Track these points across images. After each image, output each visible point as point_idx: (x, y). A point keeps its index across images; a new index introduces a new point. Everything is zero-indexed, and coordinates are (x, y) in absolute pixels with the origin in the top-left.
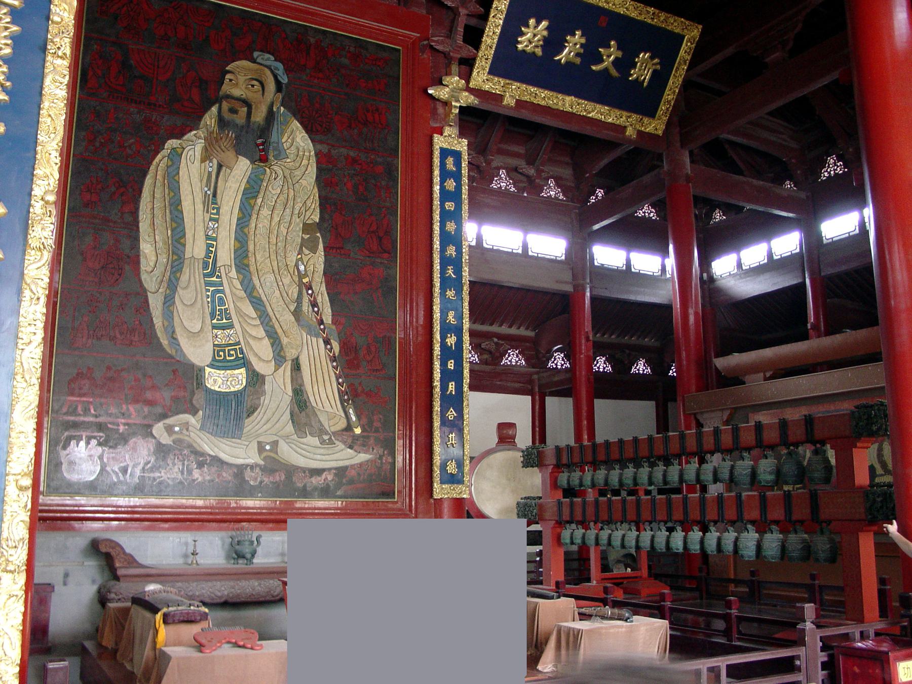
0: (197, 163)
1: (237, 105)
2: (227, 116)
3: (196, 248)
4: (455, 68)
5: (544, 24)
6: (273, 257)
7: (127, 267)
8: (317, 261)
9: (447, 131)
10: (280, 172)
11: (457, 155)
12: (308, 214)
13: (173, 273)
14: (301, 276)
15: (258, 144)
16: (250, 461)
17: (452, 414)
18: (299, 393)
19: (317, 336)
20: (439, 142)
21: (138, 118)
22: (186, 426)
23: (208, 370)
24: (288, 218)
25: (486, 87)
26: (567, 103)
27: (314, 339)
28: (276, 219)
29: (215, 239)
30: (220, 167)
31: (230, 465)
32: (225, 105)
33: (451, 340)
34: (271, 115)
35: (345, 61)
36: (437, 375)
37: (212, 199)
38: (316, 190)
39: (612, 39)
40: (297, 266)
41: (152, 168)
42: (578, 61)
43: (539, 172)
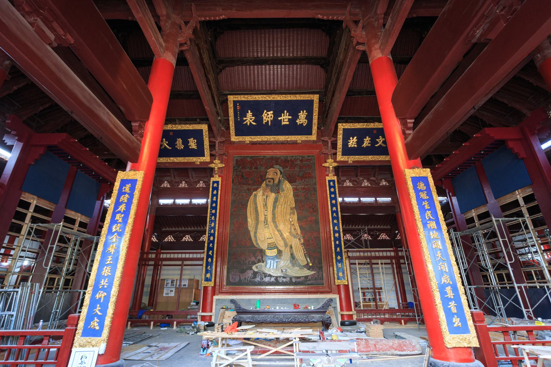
2: (268, 183)
3: (262, 218)
4: (330, 157)
5: (355, 138)
8: (295, 217)
9: (330, 175)
11: (334, 181)
15: (276, 188)
16: (279, 275)
17: (339, 258)
18: (292, 255)
20: (328, 178)
21: (246, 188)
25: (342, 160)
26: (370, 158)
33: (337, 235)
35: (299, 162)
36: (333, 246)
37: (265, 205)
42: (370, 145)
43: (377, 178)
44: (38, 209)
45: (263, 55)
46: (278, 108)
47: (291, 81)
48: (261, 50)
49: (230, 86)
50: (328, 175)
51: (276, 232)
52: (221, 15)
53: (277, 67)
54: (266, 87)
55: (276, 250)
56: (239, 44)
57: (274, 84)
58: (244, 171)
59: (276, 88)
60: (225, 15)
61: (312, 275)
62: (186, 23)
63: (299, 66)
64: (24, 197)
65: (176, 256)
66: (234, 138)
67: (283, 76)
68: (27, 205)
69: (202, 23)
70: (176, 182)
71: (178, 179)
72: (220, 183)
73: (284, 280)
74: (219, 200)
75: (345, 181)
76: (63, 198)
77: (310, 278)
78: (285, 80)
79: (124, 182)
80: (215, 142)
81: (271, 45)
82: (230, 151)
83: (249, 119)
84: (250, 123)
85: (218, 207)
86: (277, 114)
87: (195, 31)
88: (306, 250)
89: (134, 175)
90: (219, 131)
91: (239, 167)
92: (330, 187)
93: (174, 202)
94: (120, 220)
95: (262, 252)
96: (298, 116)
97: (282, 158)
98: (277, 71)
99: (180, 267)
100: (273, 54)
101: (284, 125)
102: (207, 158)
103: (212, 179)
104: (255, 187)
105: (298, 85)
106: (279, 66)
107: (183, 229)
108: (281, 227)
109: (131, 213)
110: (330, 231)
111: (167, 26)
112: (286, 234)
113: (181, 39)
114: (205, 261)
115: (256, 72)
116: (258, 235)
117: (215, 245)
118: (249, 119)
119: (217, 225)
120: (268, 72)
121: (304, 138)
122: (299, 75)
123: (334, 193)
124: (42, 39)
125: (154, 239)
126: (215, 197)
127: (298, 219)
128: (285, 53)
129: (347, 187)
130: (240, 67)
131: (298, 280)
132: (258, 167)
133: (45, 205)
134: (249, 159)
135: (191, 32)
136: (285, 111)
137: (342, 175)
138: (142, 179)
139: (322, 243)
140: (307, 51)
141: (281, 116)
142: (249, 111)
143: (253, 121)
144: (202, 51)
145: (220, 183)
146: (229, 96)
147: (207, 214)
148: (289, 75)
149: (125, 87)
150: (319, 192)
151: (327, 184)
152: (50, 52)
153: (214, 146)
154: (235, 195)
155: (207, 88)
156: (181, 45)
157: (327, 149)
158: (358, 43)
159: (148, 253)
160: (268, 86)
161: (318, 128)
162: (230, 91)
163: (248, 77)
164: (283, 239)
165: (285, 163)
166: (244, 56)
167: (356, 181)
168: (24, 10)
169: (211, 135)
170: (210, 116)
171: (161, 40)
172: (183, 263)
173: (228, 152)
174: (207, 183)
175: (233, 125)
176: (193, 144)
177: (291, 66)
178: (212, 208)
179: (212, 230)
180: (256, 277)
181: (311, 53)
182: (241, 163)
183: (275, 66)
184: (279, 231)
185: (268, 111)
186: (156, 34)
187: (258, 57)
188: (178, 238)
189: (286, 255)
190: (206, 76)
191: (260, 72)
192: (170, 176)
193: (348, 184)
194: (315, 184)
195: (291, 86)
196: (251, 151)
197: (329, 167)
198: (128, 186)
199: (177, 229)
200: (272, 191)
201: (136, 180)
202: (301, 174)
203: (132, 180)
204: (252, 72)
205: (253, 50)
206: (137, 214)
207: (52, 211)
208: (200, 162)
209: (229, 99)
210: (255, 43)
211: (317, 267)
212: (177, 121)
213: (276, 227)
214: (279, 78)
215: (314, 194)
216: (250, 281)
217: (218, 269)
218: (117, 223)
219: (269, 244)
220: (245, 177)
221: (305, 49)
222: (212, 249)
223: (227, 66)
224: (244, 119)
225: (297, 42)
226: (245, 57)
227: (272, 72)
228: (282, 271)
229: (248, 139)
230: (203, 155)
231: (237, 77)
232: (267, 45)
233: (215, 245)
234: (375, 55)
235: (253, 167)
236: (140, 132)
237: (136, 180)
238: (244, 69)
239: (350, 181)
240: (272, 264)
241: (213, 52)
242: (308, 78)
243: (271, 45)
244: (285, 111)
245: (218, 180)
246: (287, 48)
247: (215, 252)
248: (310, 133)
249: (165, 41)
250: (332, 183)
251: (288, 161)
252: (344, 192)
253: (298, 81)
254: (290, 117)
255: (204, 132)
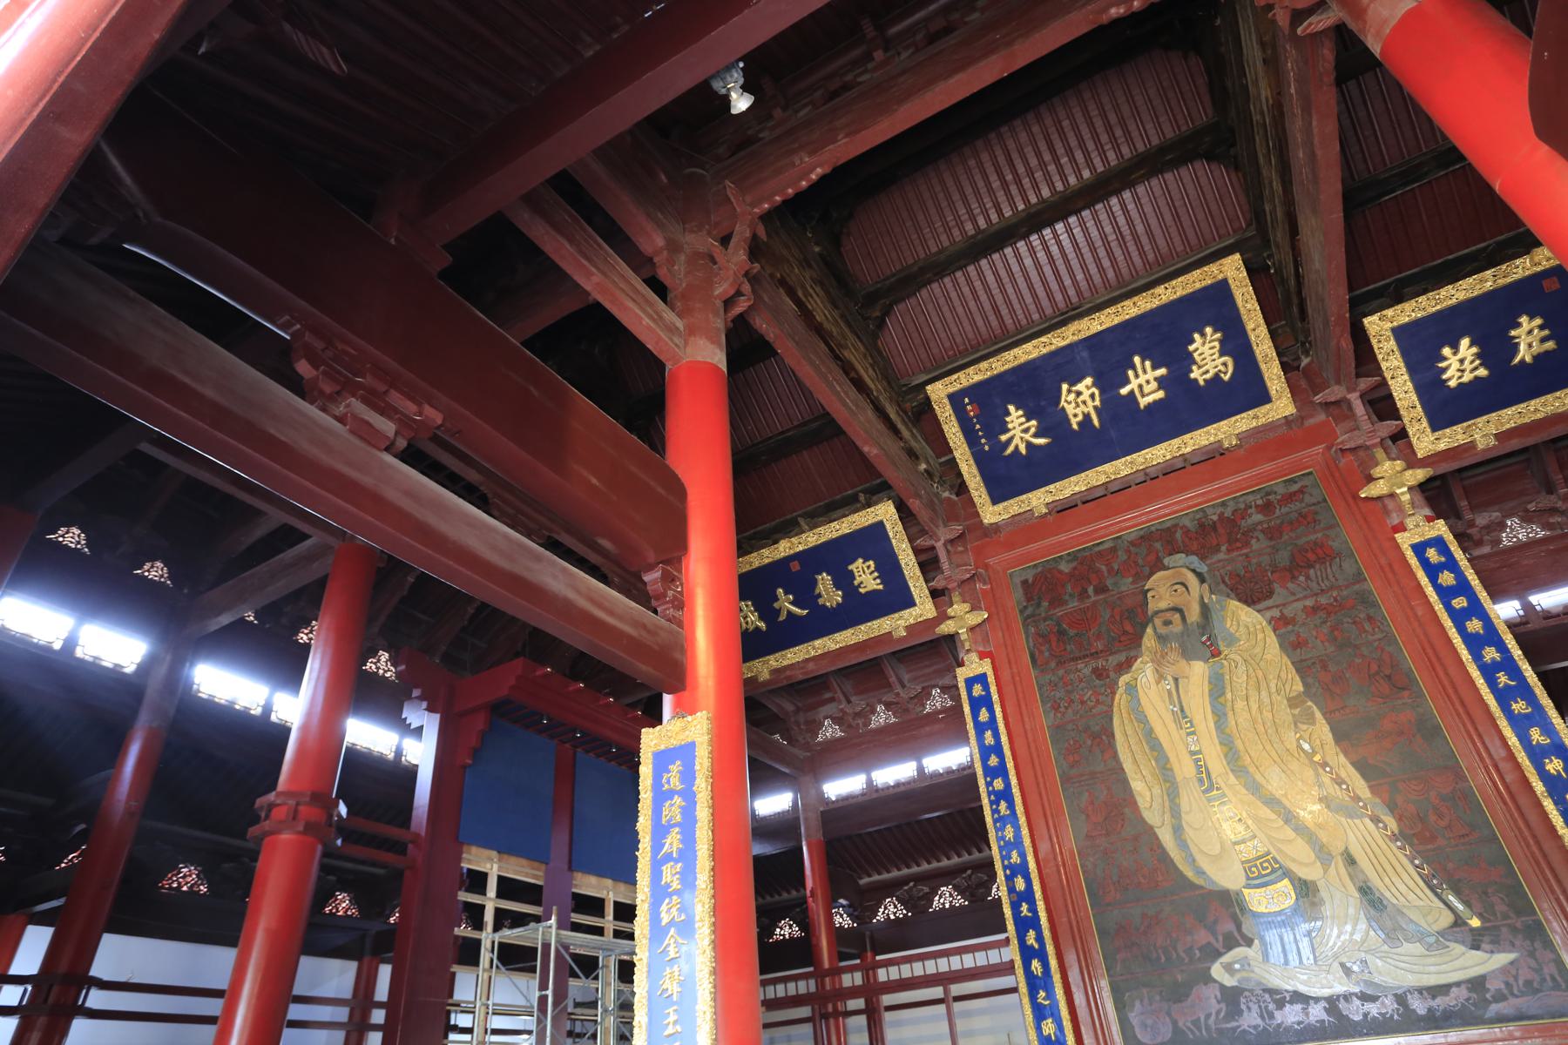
0: (1154, 686)
1: (1168, 615)
2: (1163, 630)
3: (1184, 769)
4: (1380, 454)
5: (1465, 342)
6: (1269, 747)
7: (1127, 810)
8: (1323, 730)
9: (1410, 523)
10: (1238, 658)
11: (1439, 543)
12: (1288, 687)
13: (1172, 801)
14: (1310, 756)
15: (1204, 640)
16: (1339, 988)
18: (1365, 891)
19: (1361, 817)
20: (1405, 540)
21: (1087, 671)
22: (1245, 961)
23: (1246, 891)
24: (1267, 700)
25: (1442, 446)
27: (1357, 821)
28: (1254, 707)
29: (1200, 752)
30: (1176, 680)
31: (1317, 1000)
32: (1158, 622)
34: (1205, 610)
37: (1182, 714)
38: (1285, 659)
39: (1443, 346)
40: (1299, 747)
41: (1115, 709)
42: (1550, 345)
44: (508, 888)
45: (994, 217)
46: (1105, 359)
47: (1118, 252)
48: (982, 205)
49: (924, 356)
50: (1401, 528)
51: (1266, 812)
52: (811, 171)
53: (1055, 233)
54: (1040, 309)
55: (1286, 881)
56: (909, 224)
57: (1063, 289)
58: (1059, 612)
59: (1075, 300)
60: (820, 165)
61: (1504, 970)
62: (725, 241)
63: (1127, 195)
64: (469, 861)
65: (918, 969)
66: (992, 514)
67: (1086, 250)
68: (477, 881)
69: (765, 218)
70: (857, 715)
71: (859, 703)
72: (991, 679)
73: (1373, 1009)
74: (1004, 739)
75: (1502, 526)
76: (559, 844)
77: (1494, 985)
78: (1097, 260)
79: (663, 760)
80: (933, 548)
81: (1009, 177)
82: (991, 561)
83: (1017, 432)
84: (1029, 445)
85: (1010, 765)
86: (1110, 379)
87: (755, 250)
88: (1426, 859)
89: (684, 729)
90: (936, 505)
91: (1039, 605)
92: (1432, 571)
93: (921, 769)
94: (676, 885)
95: (1229, 903)
96: (1190, 355)
97: (1187, 522)
98: (1059, 243)
99: (942, 1008)
100: (1026, 200)
101: (1149, 406)
102: (924, 608)
103: (962, 674)
104: (1122, 657)
105: (1151, 257)
106: (1060, 227)
107: (925, 866)
108: (1275, 782)
109: (699, 854)
110: (1511, 756)
111: (676, 274)
112: (1310, 810)
113: (722, 289)
114: (1019, 970)
115: (990, 278)
116: (1189, 833)
117: (1041, 906)
118: (1020, 430)
119: (1025, 832)
120: (1028, 262)
121: (1243, 422)
122: (1137, 221)
123: (1463, 587)
124: (369, 443)
125: (842, 920)
126: (988, 734)
127: (1340, 737)
128: (1064, 178)
129: (1521, 547)
130: (935, 285)
131: (1440, 1002)
132: (1109, 582)
133: (523, 871)
134: (1065, 567)
135: (742, 256)
136: (1137, 360)
137: (1473, 508)
138: (706, 738)
139: (1497, 818)
140: (1135, 134)
141: (1127, 382)
142: (1011, 408)
143: (1036, 435)
144: (800, 294)
145: (991, 679)
146: (929, 388)
147: (979, 798)
148: (1104, 237)
149: (594, 481)
150: (1387, 606)
151: (1413, 561)
152: (390, 466)
153: (936, 560)
154: (1056, 707)
155: (853, 392)
156: (728, 303)
157: (1357, 428)
158: (1298, 16)
159: (837, 972)
160: (1045, 303)
161: (1285, 367)
162: (930, 372)
163: (972, 304)
164: (1301, 829)
165: (1202, 537)
166: (934, 249)
167: (1553, 511)
168: (322, 392)
169: (914, 530)
170: (890, 474)
171: (669, 316)
172: (946, 991)
173: (986, 567)
174: (950, 690)
175: (975, 470)
176: (866, 577)
177: (1099, 206)
178: (992, 773)
179: (1014, 854)
180: (1240, 1013)
181: (1150, 135)
182: (1043, 588)
183: (1047, 232)
184: (1272, 802)
185: (1073, 383)
186: (651, 305)
187: (979, 231)
188: (917, 904)
189: (1339, 896)
190: (837, 357)
191: (1003, 273)
192: (832, 700)
193: (1517, 532)
194: (1358, 577)
195: (1125, 271)
196: (1062, 537)
197: (1392, 495)
198: (675, 768)
199: (905, 871)
200: (1188, 655)
201: (692, 746)
202: (1283, 557)
203: (681, 747)
204: (977, 284)
205: (957, 217)
206: (715, 854)
207: (540, 887)
208: (907, 628)
209: (933, 397)
210: (956, 197)
211: (1514, 930)
212: (802, 521)
213: (1255, 788)
214: (1075, 263)
215: (1370, 618)
216: (1220, 1031)
217: (1079, 999)
218: (670, 895)
219: (1248, 865)
220: (1072, 632)
221: (1127, 132)
222: (1034, 923)
223: (897, 302)
224: (1004, 438)
225: (1091, 125)
226: (940, 252)
227: (1041, 255)
228: (1348, 971)
229: (1038, 500)
230: (911, 603)
231: (936, 319)
232: (996, 184)
233: (1041, 906)
234: (1385, 13)
235: (1091, 590)
236: (670, 593)
237: (692, 746)
238: (949, 285)
239: (1527, 519)
240: (1291, 948)
241: (837, 279)
242: (1177, 217)
243: (1009, 177)
244: (1137, 360)
245: (980, 671)
246: (1064, 160)
247: (1047, 933)
248: (1262, 397)
249: (680, 316)
250: (1432, 554)
251: (1214, 526)
252: (1507, 575)
253: (1145, 240)
254: (1162, 371)
255: (888, 527)
